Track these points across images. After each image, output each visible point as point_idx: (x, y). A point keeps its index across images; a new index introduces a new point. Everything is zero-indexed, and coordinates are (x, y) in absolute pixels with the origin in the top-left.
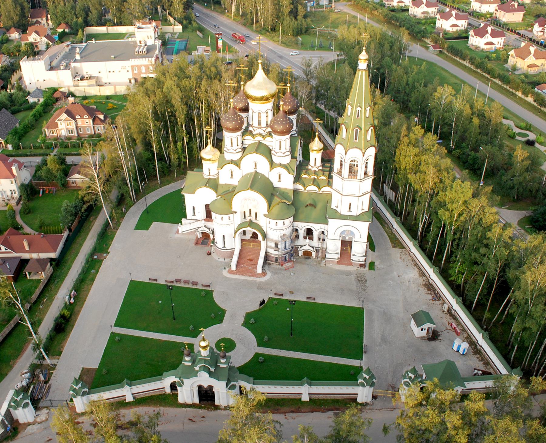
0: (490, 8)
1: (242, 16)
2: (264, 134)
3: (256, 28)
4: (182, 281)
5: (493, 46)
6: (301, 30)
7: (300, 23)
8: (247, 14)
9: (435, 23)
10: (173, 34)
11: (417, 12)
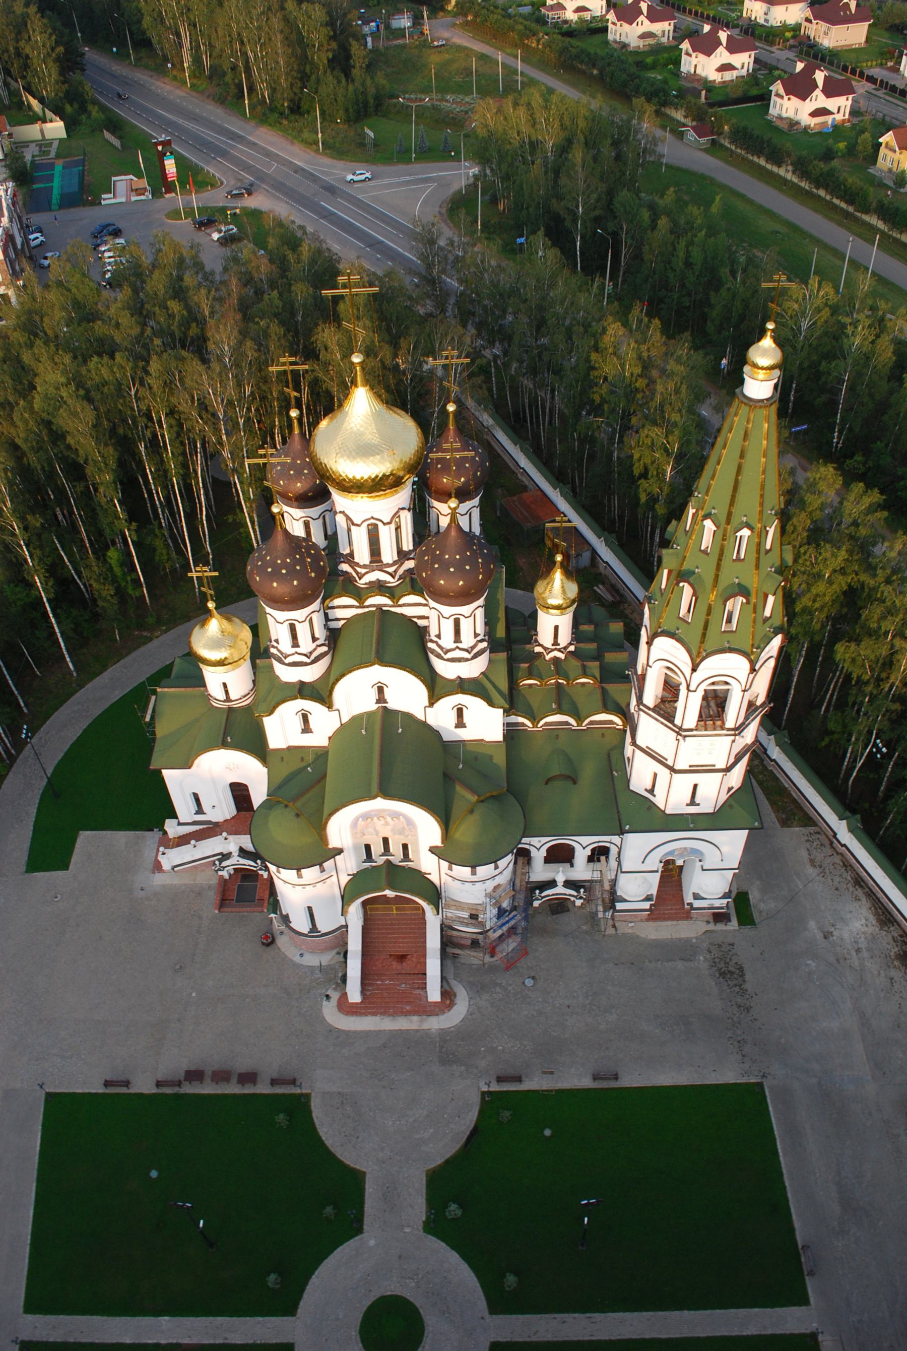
0: (792, 14)
1: (210, 77)
2: (392, 582)
3: (252, 108)
4: (208, 1073)
5: (829, 119)
6: (366, 105)
7: (361, 89)
8: (224, 74)
9: (677, 62)
10: (44, 144)
11: (630, 34)
